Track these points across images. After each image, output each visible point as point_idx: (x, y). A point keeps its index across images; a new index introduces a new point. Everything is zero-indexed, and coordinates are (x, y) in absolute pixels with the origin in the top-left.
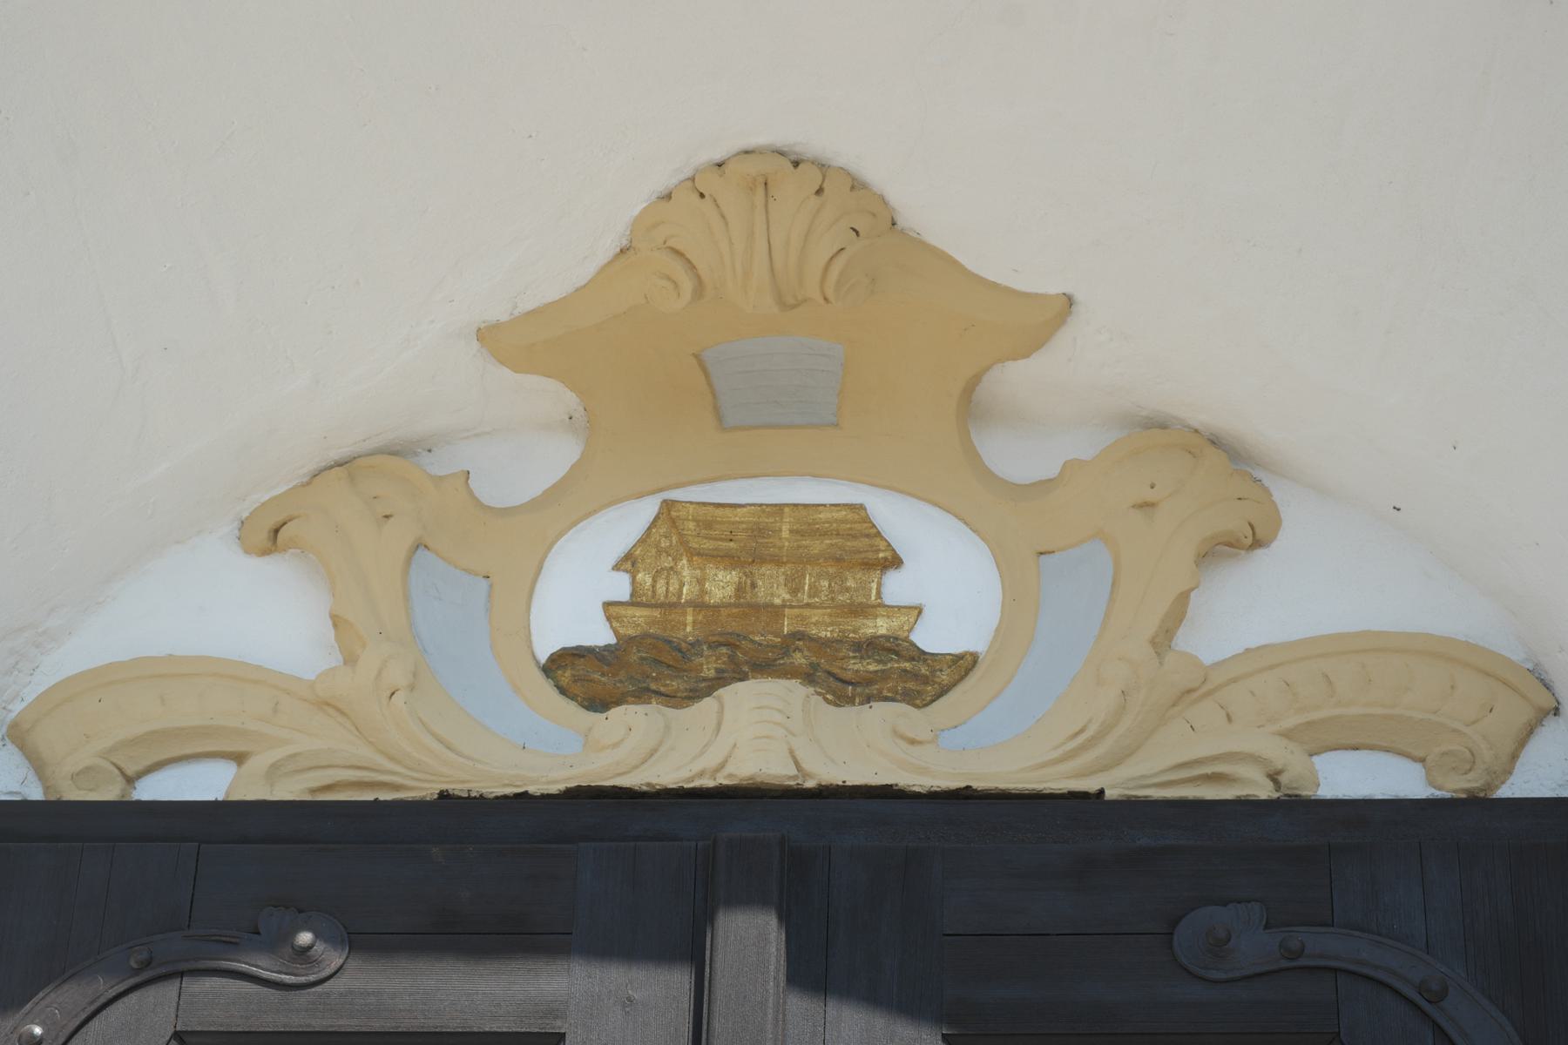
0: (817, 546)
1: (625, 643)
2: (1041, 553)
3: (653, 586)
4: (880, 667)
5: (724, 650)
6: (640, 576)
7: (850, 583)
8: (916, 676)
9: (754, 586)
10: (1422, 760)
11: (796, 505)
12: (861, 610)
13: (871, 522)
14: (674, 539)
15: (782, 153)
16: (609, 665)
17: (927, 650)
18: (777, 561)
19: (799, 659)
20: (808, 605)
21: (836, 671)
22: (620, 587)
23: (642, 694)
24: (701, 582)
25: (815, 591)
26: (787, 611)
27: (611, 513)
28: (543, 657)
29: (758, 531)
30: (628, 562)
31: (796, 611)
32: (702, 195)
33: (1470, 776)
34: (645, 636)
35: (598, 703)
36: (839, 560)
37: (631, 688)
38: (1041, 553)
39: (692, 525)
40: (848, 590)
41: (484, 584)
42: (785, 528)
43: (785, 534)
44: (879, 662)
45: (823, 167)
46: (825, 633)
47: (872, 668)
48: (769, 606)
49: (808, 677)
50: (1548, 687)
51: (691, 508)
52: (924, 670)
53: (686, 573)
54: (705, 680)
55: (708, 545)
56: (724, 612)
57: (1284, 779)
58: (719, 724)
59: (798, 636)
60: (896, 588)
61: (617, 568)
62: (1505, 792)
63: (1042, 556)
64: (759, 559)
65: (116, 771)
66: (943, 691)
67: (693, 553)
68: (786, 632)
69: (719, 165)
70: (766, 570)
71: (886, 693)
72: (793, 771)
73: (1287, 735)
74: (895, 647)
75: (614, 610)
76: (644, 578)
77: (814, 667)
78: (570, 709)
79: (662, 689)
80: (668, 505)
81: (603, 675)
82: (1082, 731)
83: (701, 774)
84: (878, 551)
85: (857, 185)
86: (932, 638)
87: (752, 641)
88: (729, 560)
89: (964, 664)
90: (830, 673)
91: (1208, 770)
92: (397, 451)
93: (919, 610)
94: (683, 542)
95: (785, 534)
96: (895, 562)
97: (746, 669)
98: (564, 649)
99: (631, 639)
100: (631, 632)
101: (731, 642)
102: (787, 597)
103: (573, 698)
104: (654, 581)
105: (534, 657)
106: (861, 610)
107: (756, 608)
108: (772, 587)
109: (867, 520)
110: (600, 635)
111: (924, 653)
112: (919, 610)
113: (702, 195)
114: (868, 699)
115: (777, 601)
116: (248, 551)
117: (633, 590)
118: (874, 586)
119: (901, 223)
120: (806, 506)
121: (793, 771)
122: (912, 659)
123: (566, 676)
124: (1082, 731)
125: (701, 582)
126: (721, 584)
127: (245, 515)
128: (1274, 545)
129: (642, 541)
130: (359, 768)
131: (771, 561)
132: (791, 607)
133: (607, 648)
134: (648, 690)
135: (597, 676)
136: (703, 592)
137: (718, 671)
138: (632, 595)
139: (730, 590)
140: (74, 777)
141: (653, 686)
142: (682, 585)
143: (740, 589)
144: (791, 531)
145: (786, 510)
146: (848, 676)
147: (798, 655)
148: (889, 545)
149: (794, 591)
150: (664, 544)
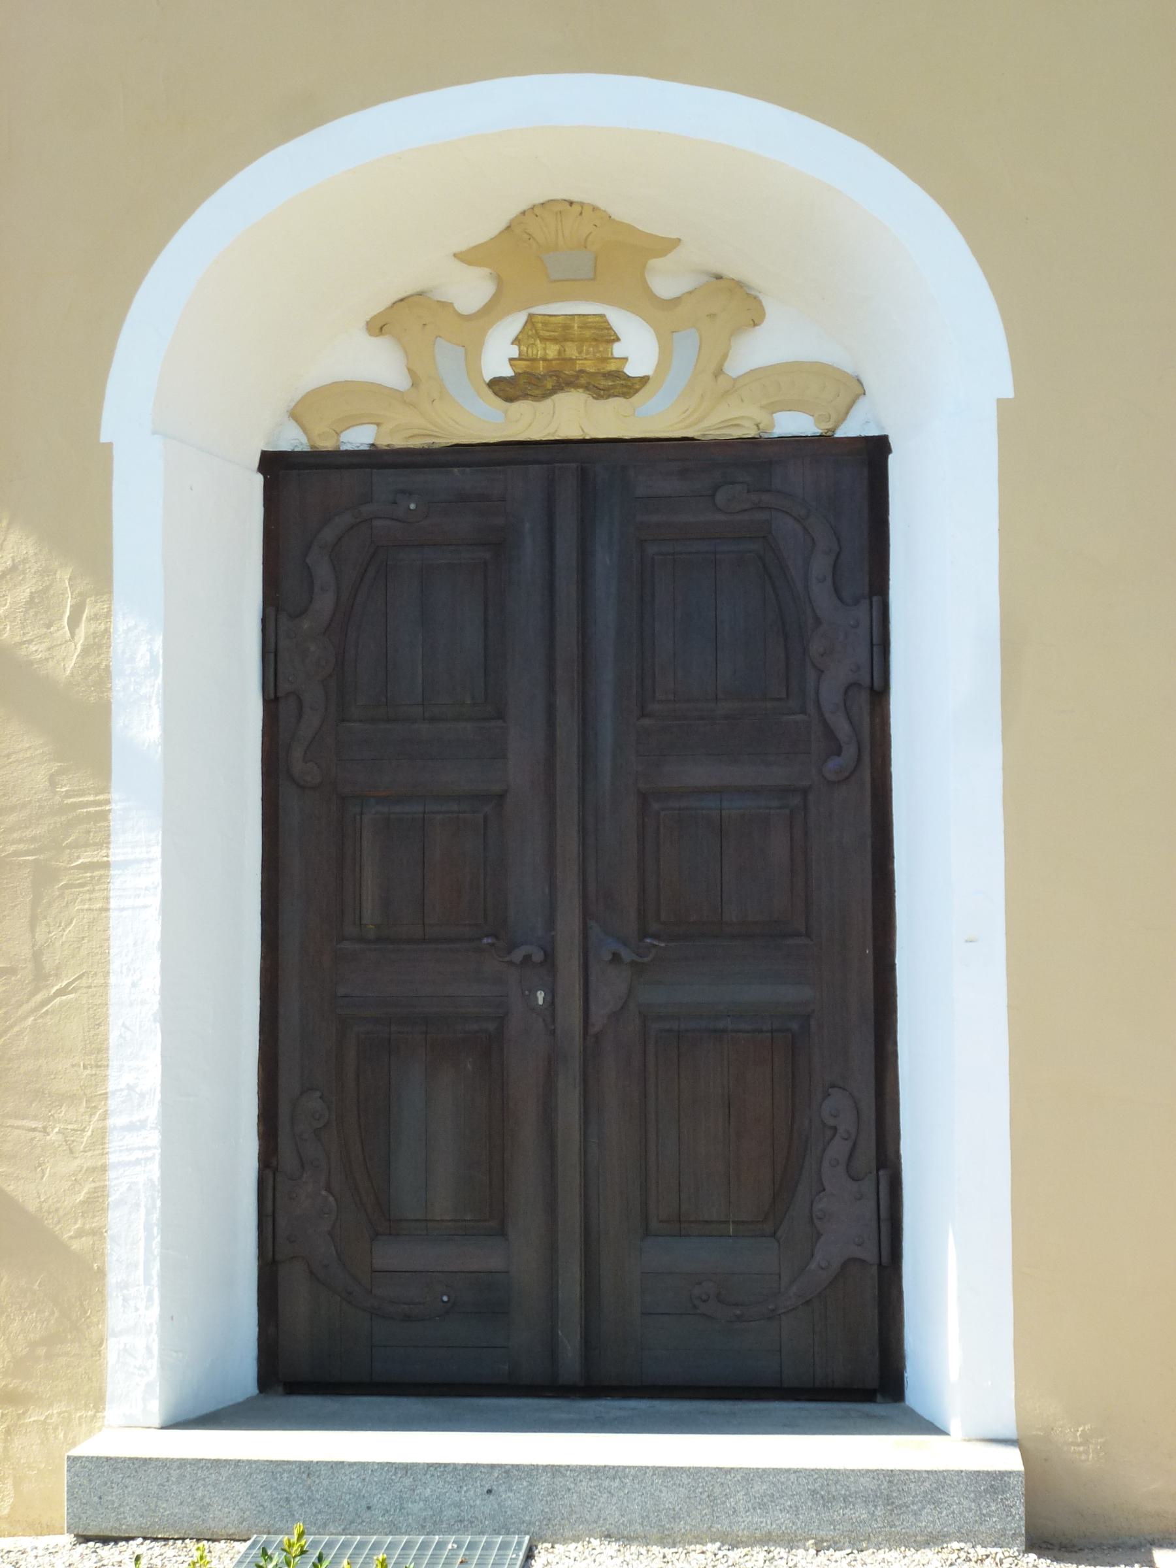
0: (588, 333)
1: (517, 375)
2: (673, 332)
3: (527, 351)
4: (613, 383)
5: (555, 378)
6: (522, 347)
7: (601, 349)
8: (627, 386)
9: (565, 351)
10: (813, 416)
11: (580, 315)
12: (605, 360)
13: (608, 322)
14: (534, 331)
15: (565, 200)
16: (513, 384)
17: (630, 375)
18: (572, 340)
19: (583, 381)
20: (585, 359)
21: (596, 385)
22: (514, 352)
23: (525, 396)
24: (545, 349)
25: (588, 353)
26: (578, 362)
27: (509, 319)
28: (487, 380)
29: (566, 327)
30: (517, 341)
31: (581, 362)
32: (537, 216)
33: (830, 423)
34: (525, 373)
35: (510, 399)
36: (596, 340)
37: (521, 394)
38: (673, 332)
39: (540, 325)
40: (600, 351)
41: (463, 348)
42: (576, 325)
43: (576, 328)
44: (613, 381)
45: (582, 204)
46: (592, 370)
47: (610, 384)
48: (571, 359)
49: (586, 388)
50: (861, 384)
51: (540, 317)
52: (629, 384)
53: (539, 345)
54: (548, 390)
55: (547, 334)
56: (554, 362)
57: (761, 426)
58: (554, 413)
59: (582, 371)
60: (618, 350)
61: (512, 343)
62: (839, 434)
63: (674, 334)
64: (566, 339)
65: (334, 432)
66: (637, 391)
67: (544, 339)
68: (486, 1537)
69: (542, 204)
70: (569, 344)
71: (616, 394)
72: (582, 433)
73: (762, 407)
74: (618, 375)
75: (513, 362)
76: (524, 348)
77: (589, 383)
78: (499, 402)
79: (533, 394)
80: (531, 316)
81: (511, 388)
82: (688, 410)
83: (549, 434)
84: (611, 336)
85: (595, 209)
86: (633, 370)
87: (565, 374)
88: (554, 340)
89: (644, 380)
90: (594, 386)
91: (734, 423)
92: (420, 294)
93: (626, 359)
94: (537, 333)
95: (576, 328)
96: (618, 339)
97: (563, 385)
98: (495, 378)
99: (520, 374)
100: (520, 371)
101: (556, 374)
102: (577, 355)
103: (500, 397)
104: (527, 349)
105: (483, 379)
106: (605, 360)
107: (564, 359)
108: (571, 351)
109: (607, 322)
110: (508, 372)
111: (629, 377)
112: (626, 359)
113: (537, 216)
114: (609, 396)
115: (574, 357)
116: (371, 335)
117: (520, 352)
118: (610, 350)
119: (613, 217)
120: (584, 315)
121: (582, 433)
122: (624, 380)
123: (497, 388)
124: (688, 410)
125: (545, 349)
126: (552, 351)
127: (368, 320)
128: (762, 325)
129: (521, 332)
130: (423, 429)
131: (570, 341)
132: (579, 359)
133: (511, 378)
134: (528, 395)
135: (508, 389)
136: (546, 354)
137: (553, 386)
138: (519, 354)
139: (556, 353)
140: (319, 435)
141: (529, 393)
142: (538, 351)
143: (559, 352)
144: (578, 327)
145: (576, 317)
146: (601, 387)
147: (582, 379)
148: (615, 333)
149: (580, 353)
150: (530, 333)
